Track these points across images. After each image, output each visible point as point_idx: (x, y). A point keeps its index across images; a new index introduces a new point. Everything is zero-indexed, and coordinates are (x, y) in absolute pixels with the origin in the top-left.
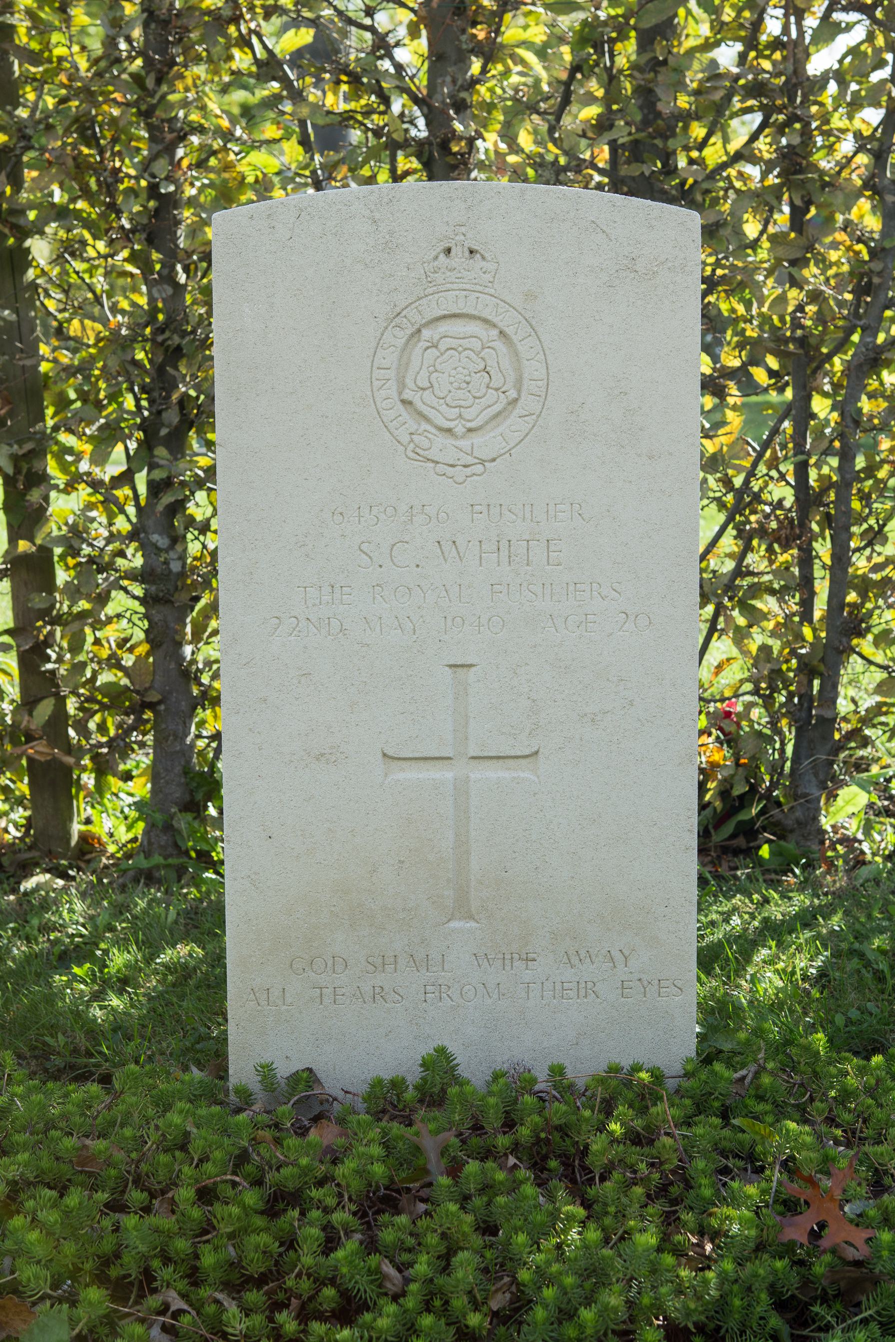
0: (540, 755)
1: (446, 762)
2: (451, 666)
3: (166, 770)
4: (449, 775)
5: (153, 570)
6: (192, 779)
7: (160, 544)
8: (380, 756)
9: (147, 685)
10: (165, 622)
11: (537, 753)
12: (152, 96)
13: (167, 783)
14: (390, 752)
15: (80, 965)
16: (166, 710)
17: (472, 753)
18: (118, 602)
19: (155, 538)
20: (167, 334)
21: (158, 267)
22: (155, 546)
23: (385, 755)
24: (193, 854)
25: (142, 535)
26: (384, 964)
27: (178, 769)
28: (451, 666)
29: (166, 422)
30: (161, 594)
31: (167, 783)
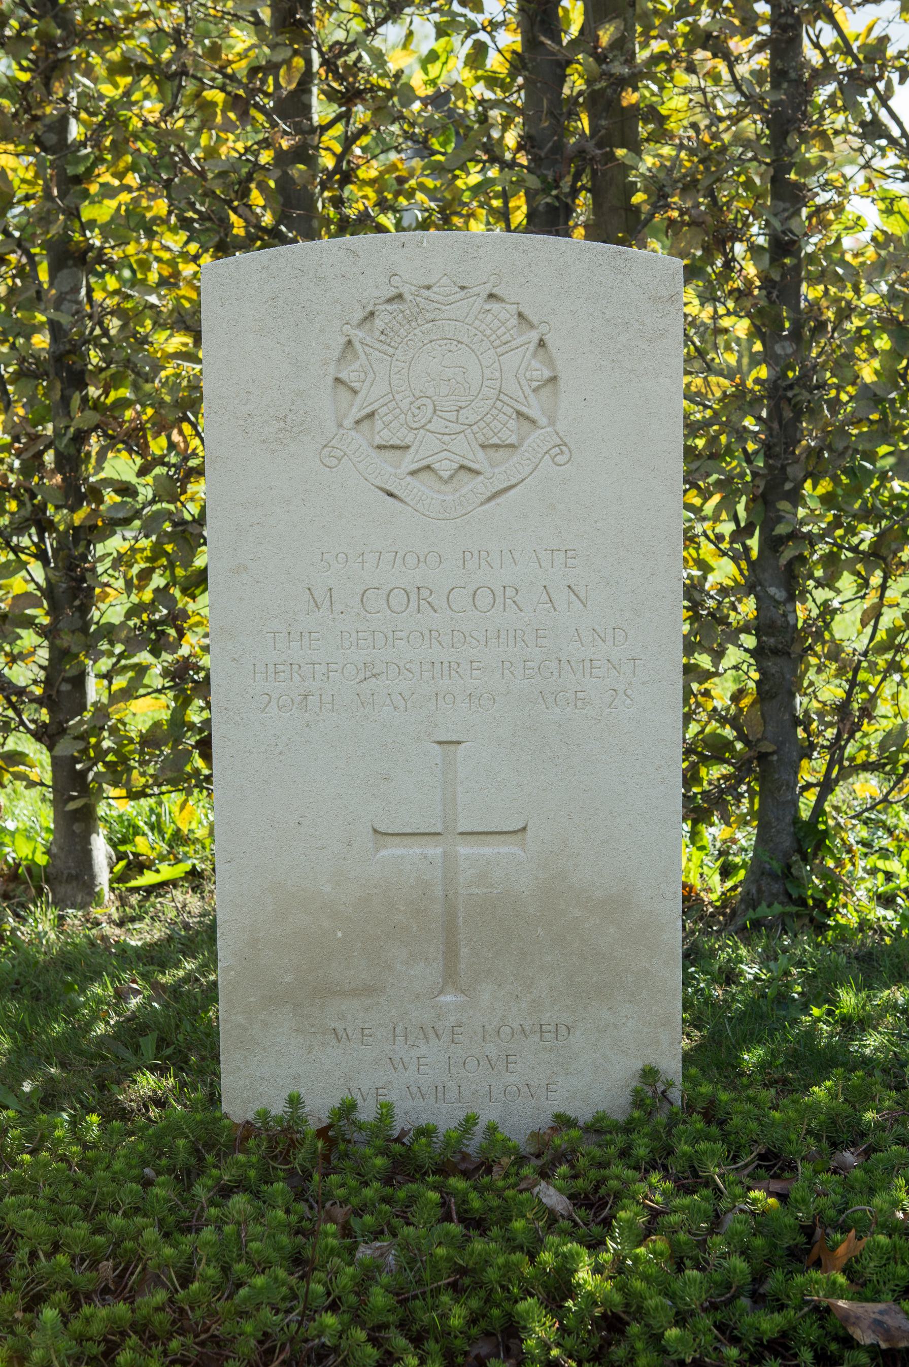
0: (530, 833)
1: (436, 838)
2: (440, 743)
3: (778, 819)
4: (439, 850)
5: (773, 622)
6: (800, 829)
7: (777, 597)
8: (371, 832)
9: (759, 736)
10: (782, 674)
11: (524, 829)
12: (540, 148)
13: (778, 832)
14: (377, 827)
15: (819, 1006)
16: (778, 760)
17: (460, 830)
18: (733, 655)
19: (772, 590)
20: (796, 390)
21: (787, 325)
22: (772, 598)
23: (375, 831)
24: (811, 902)
25: (758, 588)
26: (395, 1036)
27: (788, 819)
28: (440, 743)
29: (791, 476)
30: (780, 646)
31: (778, 832)
